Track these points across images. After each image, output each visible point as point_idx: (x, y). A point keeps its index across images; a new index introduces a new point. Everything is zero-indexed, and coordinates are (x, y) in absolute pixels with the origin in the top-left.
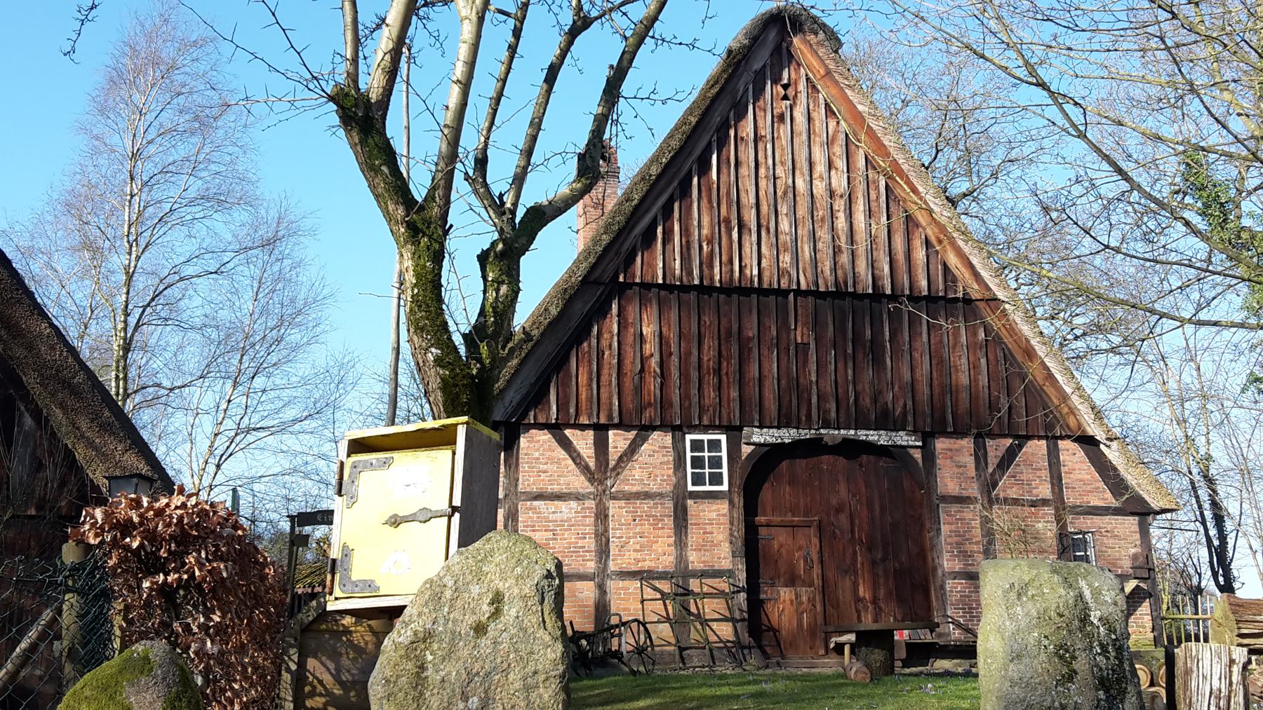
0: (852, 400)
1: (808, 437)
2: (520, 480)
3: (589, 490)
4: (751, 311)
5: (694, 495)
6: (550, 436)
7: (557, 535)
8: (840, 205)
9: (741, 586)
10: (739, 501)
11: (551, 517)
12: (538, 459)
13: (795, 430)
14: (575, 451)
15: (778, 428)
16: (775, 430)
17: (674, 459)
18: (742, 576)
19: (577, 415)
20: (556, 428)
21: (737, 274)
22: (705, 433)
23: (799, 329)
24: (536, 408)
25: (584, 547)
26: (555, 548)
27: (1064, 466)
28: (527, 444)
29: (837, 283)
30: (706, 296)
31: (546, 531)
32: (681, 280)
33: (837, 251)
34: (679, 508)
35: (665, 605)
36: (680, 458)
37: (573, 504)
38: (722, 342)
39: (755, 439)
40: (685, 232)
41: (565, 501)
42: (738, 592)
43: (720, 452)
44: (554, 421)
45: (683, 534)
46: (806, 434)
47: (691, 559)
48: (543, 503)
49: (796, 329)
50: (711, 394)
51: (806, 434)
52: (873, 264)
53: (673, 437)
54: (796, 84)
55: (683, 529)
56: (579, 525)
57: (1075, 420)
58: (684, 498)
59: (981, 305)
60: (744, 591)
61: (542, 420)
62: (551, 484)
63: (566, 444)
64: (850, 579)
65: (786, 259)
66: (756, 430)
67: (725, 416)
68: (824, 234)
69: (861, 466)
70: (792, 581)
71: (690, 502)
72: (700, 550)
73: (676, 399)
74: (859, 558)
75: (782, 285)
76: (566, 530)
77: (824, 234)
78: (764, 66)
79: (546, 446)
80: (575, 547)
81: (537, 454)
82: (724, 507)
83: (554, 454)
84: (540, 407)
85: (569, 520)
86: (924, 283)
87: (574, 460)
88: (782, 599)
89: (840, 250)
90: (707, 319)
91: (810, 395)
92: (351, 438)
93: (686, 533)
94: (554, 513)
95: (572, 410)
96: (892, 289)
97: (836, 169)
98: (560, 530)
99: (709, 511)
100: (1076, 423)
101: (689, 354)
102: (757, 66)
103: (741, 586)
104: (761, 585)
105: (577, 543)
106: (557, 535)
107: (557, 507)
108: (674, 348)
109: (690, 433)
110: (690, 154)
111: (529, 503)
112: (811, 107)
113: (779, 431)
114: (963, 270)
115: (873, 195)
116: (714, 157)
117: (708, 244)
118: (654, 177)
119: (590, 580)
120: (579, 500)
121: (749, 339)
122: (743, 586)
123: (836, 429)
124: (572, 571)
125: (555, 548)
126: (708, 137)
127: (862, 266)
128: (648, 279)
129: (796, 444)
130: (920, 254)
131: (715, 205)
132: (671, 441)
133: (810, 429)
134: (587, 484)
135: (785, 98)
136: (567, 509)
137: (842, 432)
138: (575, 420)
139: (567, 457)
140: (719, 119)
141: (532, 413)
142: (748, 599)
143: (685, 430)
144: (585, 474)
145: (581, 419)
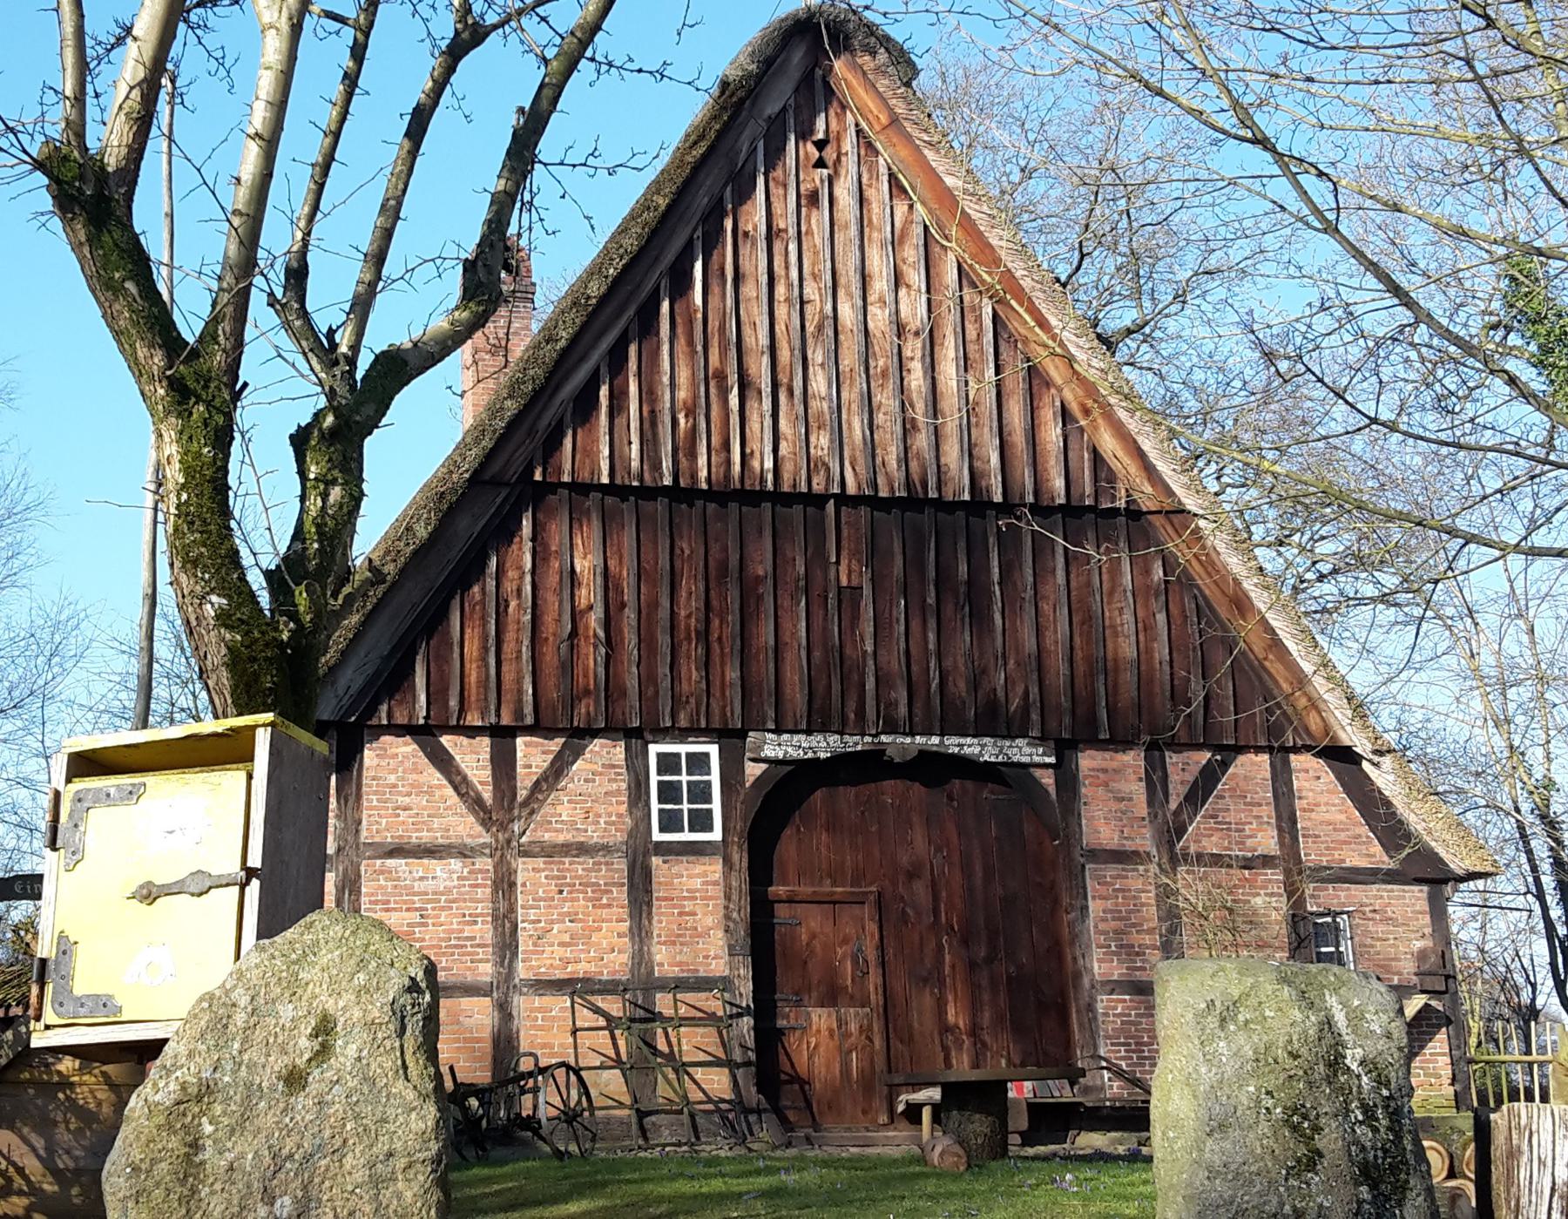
0: (935, 684)
1: (859, 748)
2: (364, 822)
3: (482, 840)
4: (760, 532)
5: (664, 849)
6: (416, 746)
9: (744, 1005)
10: (740, 858)
12: (395, 786)
13: (837, 737)
15: (809, 732)
16: (802, 737)
18: (746, 989)
20: (424, 734)
21: (737, 468)
26: (423, 940)
27: (1300, 798)
28: (376, 761)
30: (684, 506)
31: (408, 910)
34: (638, 870)
35: (613, 1038)
36: (638, 784)
37: (455, 864)
39: (769, 752)
42: (740, 1015)
46: (857, 744)
47: (658, 958)
48: (403, 861)
49: (838, 562)
50: (692, 674)
51: (856, 743)
52: (971, 451)
54: (838, 140)
55: (645, 908)
56: (465, 900)
57: (1318, 720)
58: (646, 854)
59: (1157, 521)
61: (401, 718)
62: (417, 830)
63: (443, 761)
64: (932, 993)
65: (822, 442)
66: (770, 736)
68: (886, 399)
69: (950, 798)
70: (831, 996)
71: (656, 861)
72: (674, 943)
73: (632, 683)
74: (947, 957)
77: (886, 399)
78: (784, 109)
79: (409, 764)
81: (392, 779)
82: (714, 869)
83: (422, 778)
85: (448, 891)
86: (1059, 484)
87: (456, 789)
88: (814, 1028)
89: (915, 427)
93: (650, 913)
94: (421, 879)
97: (908, 286)
101: (654, 605)
102: (772, 108)
103: (744, 1005)
107: (427, 870)
111: (379, 862)
112: (865, 180)
114: (1126, 460)
115: (971, 333)
116: (698, 266)
120: (465, 856)
121: (759, 580)
122: (748, 1006)
124: (453, 979)
125: (423, 940)
127: (952, 454)
128: (584, 476)
129: (840, 761)
130: (1052, 434)
131: (699, 348)
134: (479, 829)
135: (820, 163)
136: (445, 873)
137: (918, 739)
139: (445, 782)
140: (706, 200)
141: (384, 707)
142: (756, 1028)
145: (469, 718)
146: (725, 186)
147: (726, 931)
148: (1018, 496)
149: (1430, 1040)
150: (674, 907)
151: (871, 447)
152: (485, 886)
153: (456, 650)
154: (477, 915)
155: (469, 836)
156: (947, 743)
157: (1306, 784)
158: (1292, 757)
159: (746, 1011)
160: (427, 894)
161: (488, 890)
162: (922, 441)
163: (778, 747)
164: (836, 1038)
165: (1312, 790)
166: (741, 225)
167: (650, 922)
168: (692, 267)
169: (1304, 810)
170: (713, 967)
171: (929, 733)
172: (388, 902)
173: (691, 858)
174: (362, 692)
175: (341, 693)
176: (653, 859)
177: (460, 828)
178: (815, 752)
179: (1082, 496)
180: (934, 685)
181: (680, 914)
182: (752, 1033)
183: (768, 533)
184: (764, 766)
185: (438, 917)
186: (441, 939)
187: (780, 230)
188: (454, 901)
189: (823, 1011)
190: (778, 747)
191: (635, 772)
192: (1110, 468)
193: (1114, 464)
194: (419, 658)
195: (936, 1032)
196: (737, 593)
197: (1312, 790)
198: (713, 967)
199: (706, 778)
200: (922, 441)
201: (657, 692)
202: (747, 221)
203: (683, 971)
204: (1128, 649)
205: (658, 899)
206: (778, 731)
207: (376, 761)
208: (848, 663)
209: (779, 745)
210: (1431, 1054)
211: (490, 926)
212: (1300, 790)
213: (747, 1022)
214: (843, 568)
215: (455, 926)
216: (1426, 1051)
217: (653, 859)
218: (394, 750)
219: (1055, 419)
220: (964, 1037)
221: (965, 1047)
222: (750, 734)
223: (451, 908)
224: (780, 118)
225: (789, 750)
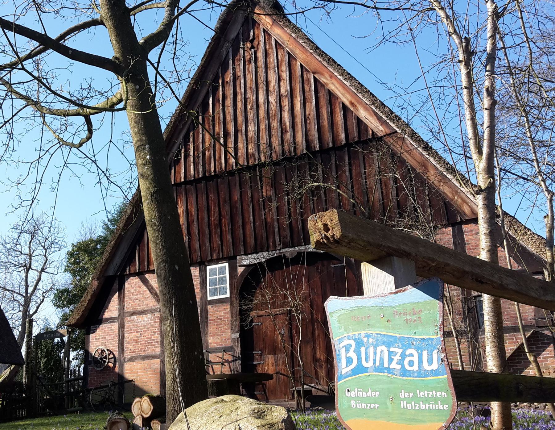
0: (300, 226)
1: (275, 255)
2: (125, 306)
3: (157, 307)
4: (235, 185)
5: (212, 302)
6: (139, 279)
7: (142, 334)
8: (286, 103)
9: (237, 356)
10: (236, 302)
11: (140, 324)
12: (133, 293)
13: (267, 253)
14: (150, 286)
15: (257, 253)
16: (255, 255)
17: (200, 283)
18: (238, 350)
19: (149, 265)
20: (141, 274)
21: (223, 165)
22: (217, 264)
23: (264, 188)
24: (130, 265)
25: (155, 339)
26: (141, 342)
27: (468, 244)
28: (128, 286)
29: (283, 153)
30: (211, 182)
31: (137, 332)
32: (194, 177)
33: (283, 132)
34: (204, 311)
35: (214, 372)
36: (203, 281)
37: (149, 315)
38: (221, 206)
39: (244, 262)
40: (196, 149)
41: (146, 314)
42: (236, 360)
43: (225, 274)
44: (138, 271)
45: (206, 326)
46: (274, 254)
47: (210, 341)
48: (135, 317)
49: (262, 188)
50: (217, 241)
51: (274, 254)
52: (306, 134)
53: (200, 269)
54: (258, 37)
55: (206, 324)
56: (152, 327)
57: (468, 207)
58: (206, 305)
59: (387, 139)
60: (239, 360)
61: (132, 271)
62: (139, 306)
63: (145, 282)
64: (310, 347)
65: (252, 148)
66: (244, 256)
67: (225, 251)
68: (275, 124)
69: (317, 269)
70: (274, 350)
71: (209, 307)
72: (214, 335)
73: (197, 246)
74: (317, 332)
75: (250, 164)
76: (146, 331)
77: (275, 124)
78: (238, 34)
79: (137, 285)
80: (151, 340)
81: (133, 291)
82: (227, 308)
83: (141, 289)
84: (132, 264)
85: (148, 324)
86: (343, 136)
87: (150, 291)
88: (267, 363)
89: (286, 131)
90: (212, 196)
91: (274, 228)
92: (361, 297)
93: (207, 325)
94: (140, 322)
95: (146, 263)
96: (320, 146)
97: (284, 80)
98: (144, 331)
99: (220, 311)
100: (469, 209)
101: (203, 219)
102: (233, 35)
103: (237, 356)
104: (255, 355)
105: (151, 338)
106: (142, 334)
107: (142, 318)
108: (195, 218)
109: (209, 265)
110: (196, 102)
111: (129, 318)
112: (267, 47)
113: (257, 255)
114: (370, 118)
115: (306, 88)
116: (211, 99)
117: (208, 151)
118: (173, 123)
119: (158, 358)
120: (152, 313)
121: (236, 202)
122: (239, 356)
123: (292, 247)
124: (149, 354)
125: (141, 342)
126: (207, 88)
127: (300, 138)
128: (178, 181)
129: (269, 262)
130: (339, 117)
131: (211, 127)
132: (198, 272)
133: (276, 250)
134: (156, 303)
135: (253, 47)
136: (146, 319)
137: (297, 248)
138: (148, 269)
139: (147, 289)
140: (211, 76)
141: (128, 269)
142: (241, 364)
143: (207, 264)
144: (154, 297)
145: (151, 267)
146: (218, 69)
147: (232, 330)
148: (327, 145)
149: (543, 351)
150: (215, 322)
151: (270, 145)
152: (158, 322)
153: (146, 246)
154: (156, 332)
155: (154, 306)
156: (307, 248)
157: (471, 237)
158: (463, 226)
159: (238, 358)
160: (142, 326)
161: (159, 323)
162: (288, 136)
163: (246, 260)
164: (274, 366)
165: (474, 239)
166: (226, 80)
167: (207, 329)
168: (209, 100)
169: (470, 249)
170: (227, 343)
171: (300, 245)
172: (131, 330)
173: (220, 305)
174: (121, 264)
175: (115, 266)
176: (208, 306)
177: (151, 304)
178: (260, 260)
179: (354, 137)
180: (300, 227)
181: (217, 325)
182: (240, 366)
183: (238, 184)
184: (244, 268)
185: (145, 333)
186: (146, 341)
187: (239, 77)
188: (149, 328)
189: (270, 357)
190: (246, 260)
191: (202, 277)
192: (365, 124)
193: (366, 121)
194: (137, 251)
195: (312, 362)
196: (228, 208)
197: (474, 239)
198: (227, 343)
199: (225, 275)
200: (288, 136)
201: (206, 248)
202: (227, 77)
203: (217, 345)
204: (377, 196)
205: (210, 320)
206: (246, 254)
207: (128, 286)
208: (268, 225)
209: (247, 259)
210: (543, 358)
211: (159, 335)
212: (468, 240)
213: (239, 362)
214: (264, 191)
215: (149, 336)
216: (541, 356)
217: (208, 306)
218: (133, 281)
219: (340, 111)
220: (323, 363)
221: (324, 367)
222: (238, 257)
223: (148, 330)
224: (237, 38)
225: (251, 260)
